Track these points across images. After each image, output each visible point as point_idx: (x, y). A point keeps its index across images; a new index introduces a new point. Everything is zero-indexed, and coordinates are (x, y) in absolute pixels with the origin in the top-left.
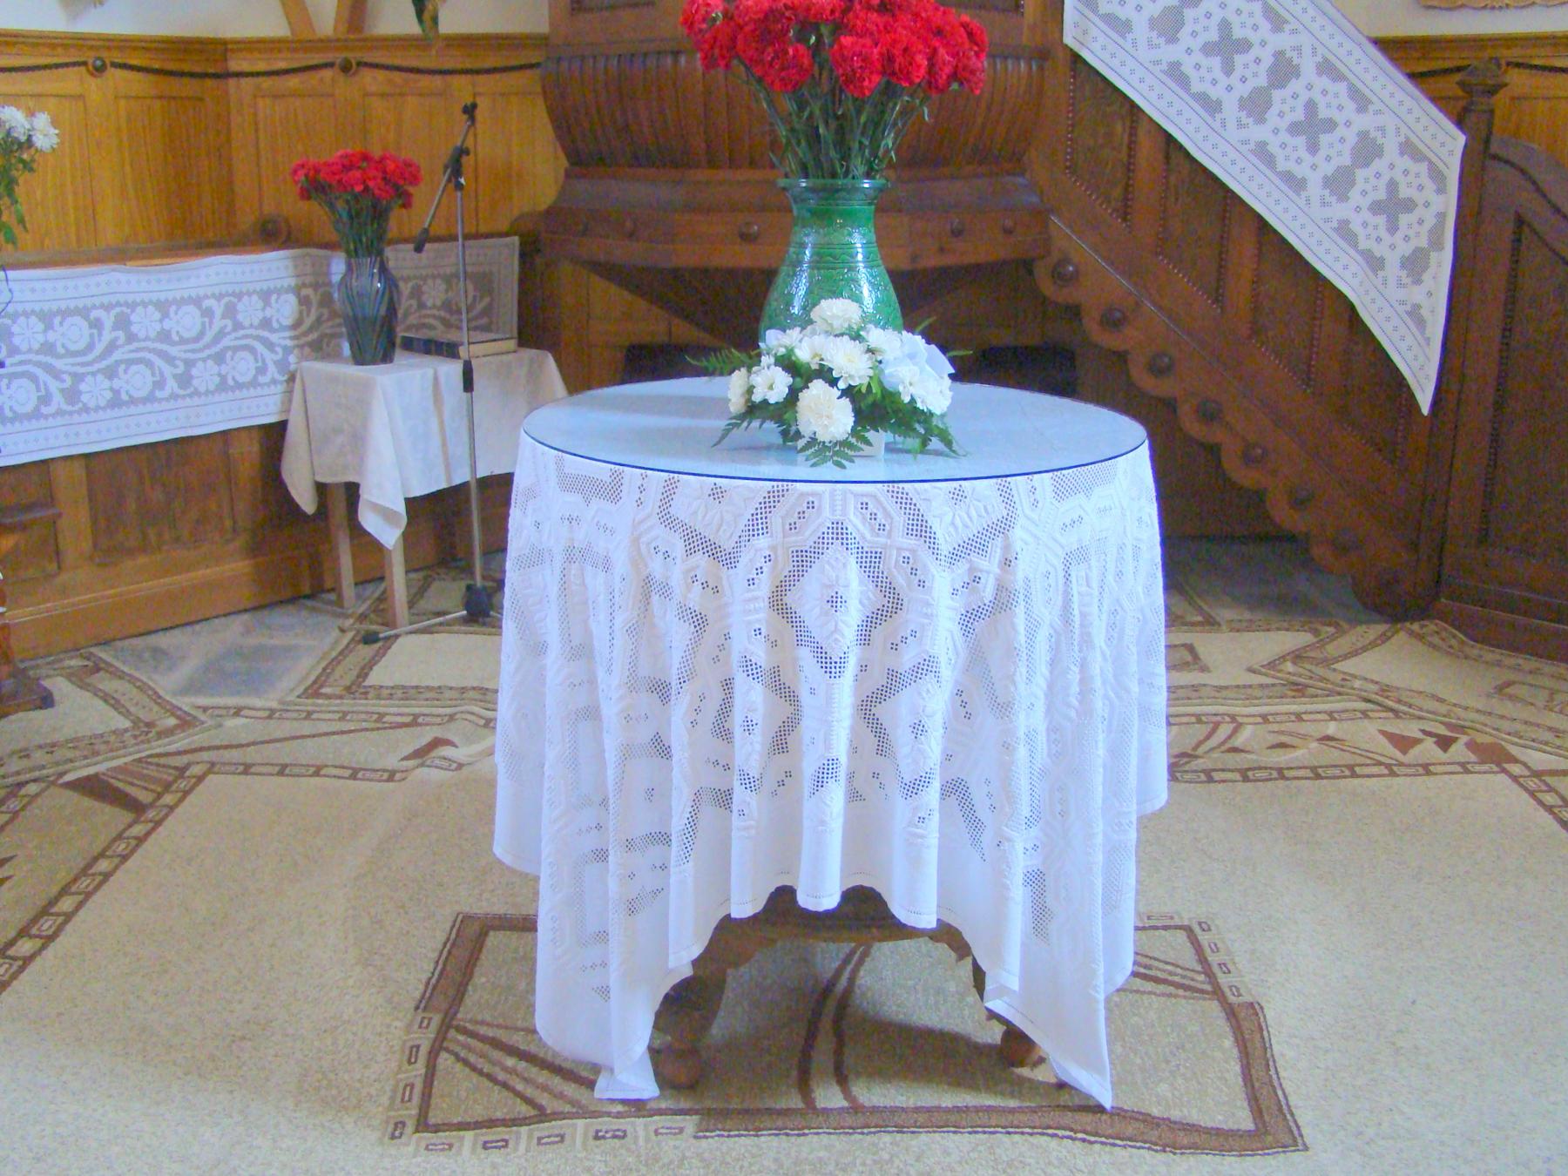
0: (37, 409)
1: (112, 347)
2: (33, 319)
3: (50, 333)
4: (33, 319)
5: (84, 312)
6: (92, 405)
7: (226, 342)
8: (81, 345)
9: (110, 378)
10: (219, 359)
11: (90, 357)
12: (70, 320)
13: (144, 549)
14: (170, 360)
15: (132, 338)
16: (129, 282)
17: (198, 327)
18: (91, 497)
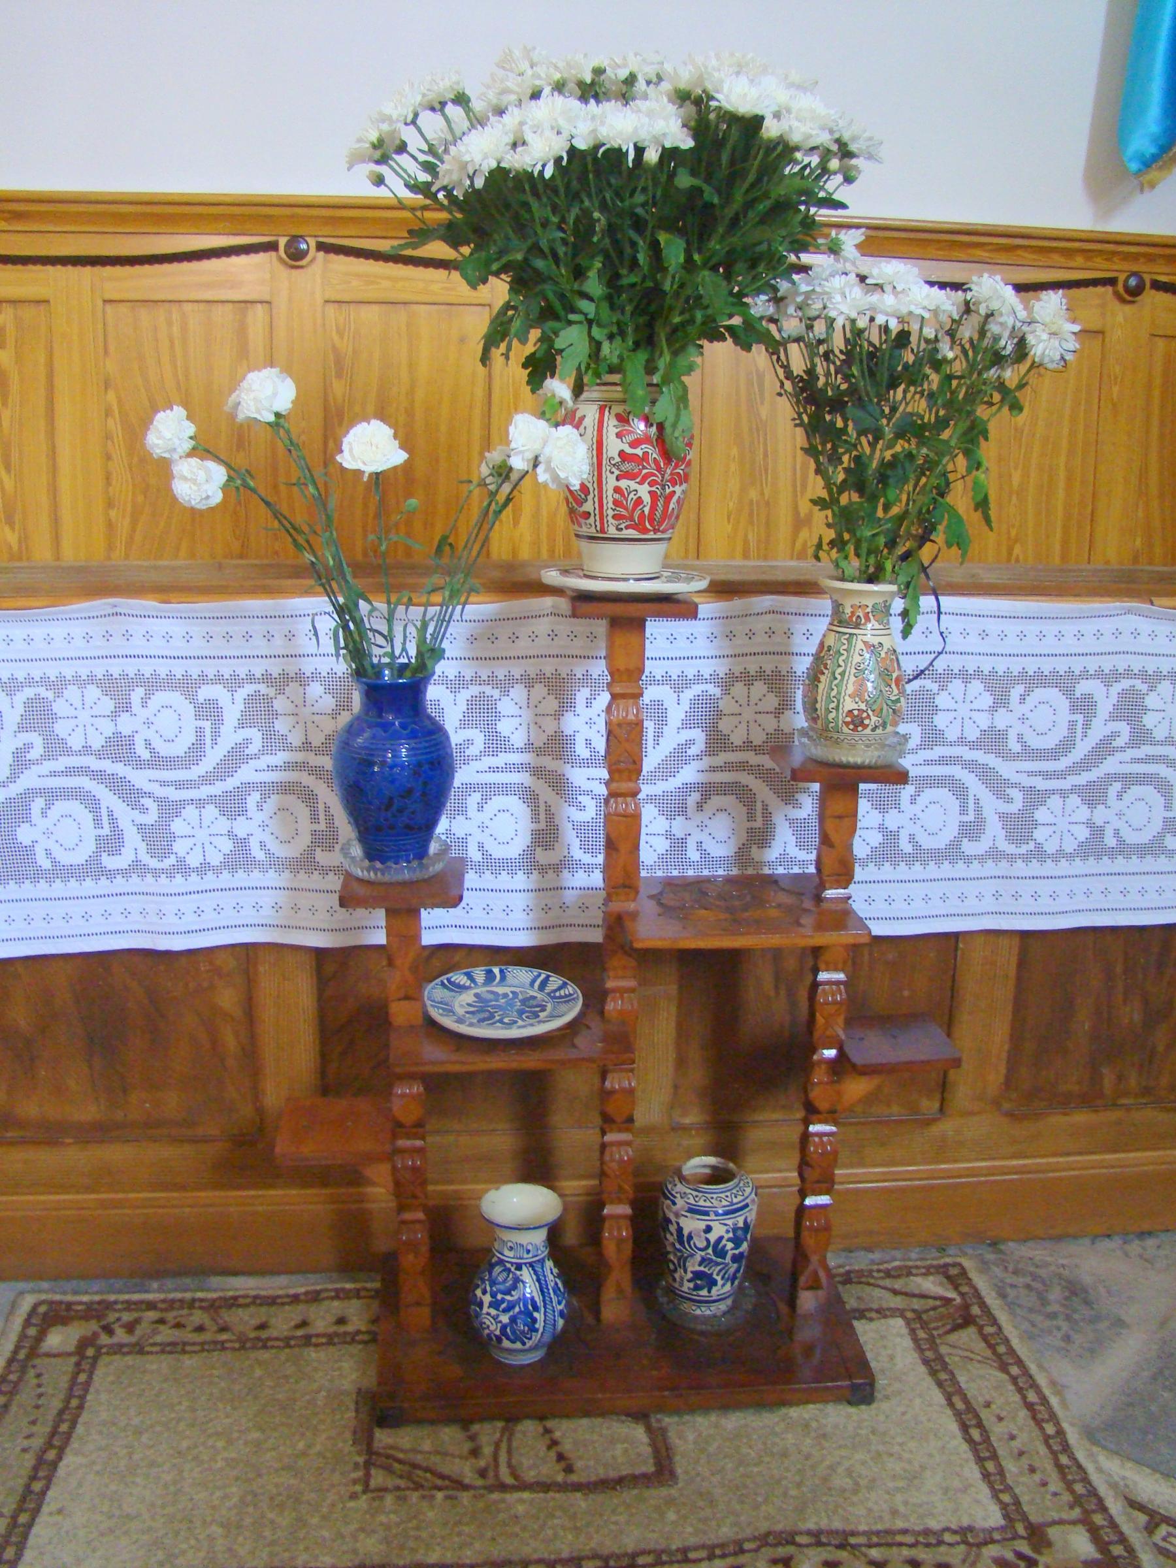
0: (955, 845)
1: (1104, 748)
2: (976, 686)
3: (125, 717)
4: (976, 686)
5: (1065, 682)
6: (1051, 847)
8: (1050, 742)
9: (1091, 803)
10: (1093, 795)
12: (1039, 694)
13: (1090, 1099)
14: (998, 786)
15: (1141, 736)
16: (1153, 635)
17: (1062, 731)
18: (1019, 1004)
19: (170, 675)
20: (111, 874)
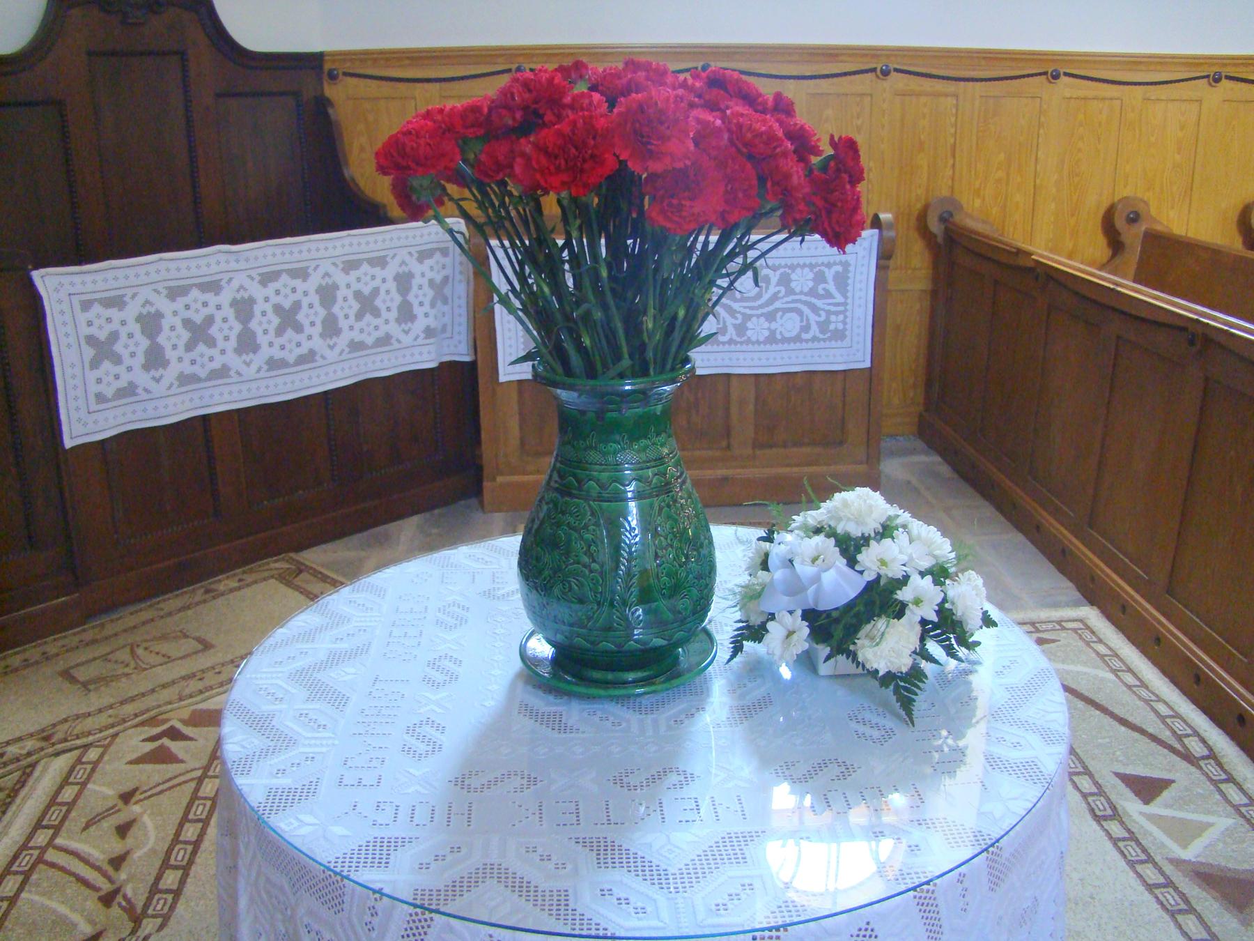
1: (775, 297)
7: (778, 304)
10: (770, 317)
14: (815, 309)
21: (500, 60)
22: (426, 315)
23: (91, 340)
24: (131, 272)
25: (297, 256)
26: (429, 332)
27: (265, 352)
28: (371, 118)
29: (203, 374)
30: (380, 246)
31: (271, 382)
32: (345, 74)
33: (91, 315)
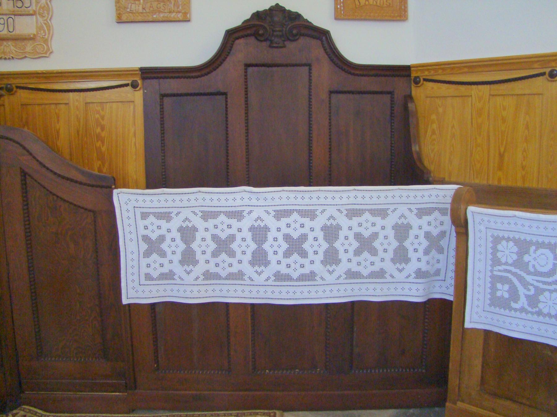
4: (511, 244)
8: (545, 269)
11: (550, 280)
19: (543, 242)
20: (511, 309)
21: (536, 66)
22: (419, 260)
23: (146, 239)
24: (177, 198)
25: (307, 201)
26: (420, 274)
27: (273, 267)
28: (441, 110)
29: (224, 274)
30: (382, 200)
31: (277, 289)
32: (425, 80)
33: (147, 222)
